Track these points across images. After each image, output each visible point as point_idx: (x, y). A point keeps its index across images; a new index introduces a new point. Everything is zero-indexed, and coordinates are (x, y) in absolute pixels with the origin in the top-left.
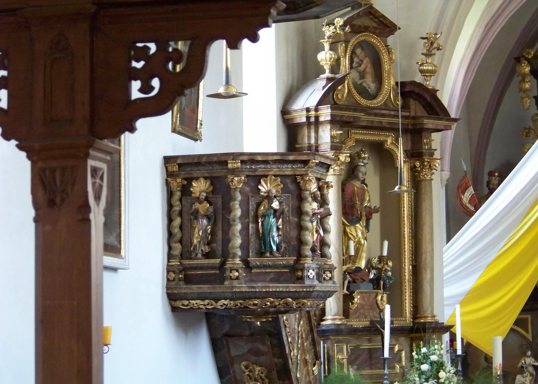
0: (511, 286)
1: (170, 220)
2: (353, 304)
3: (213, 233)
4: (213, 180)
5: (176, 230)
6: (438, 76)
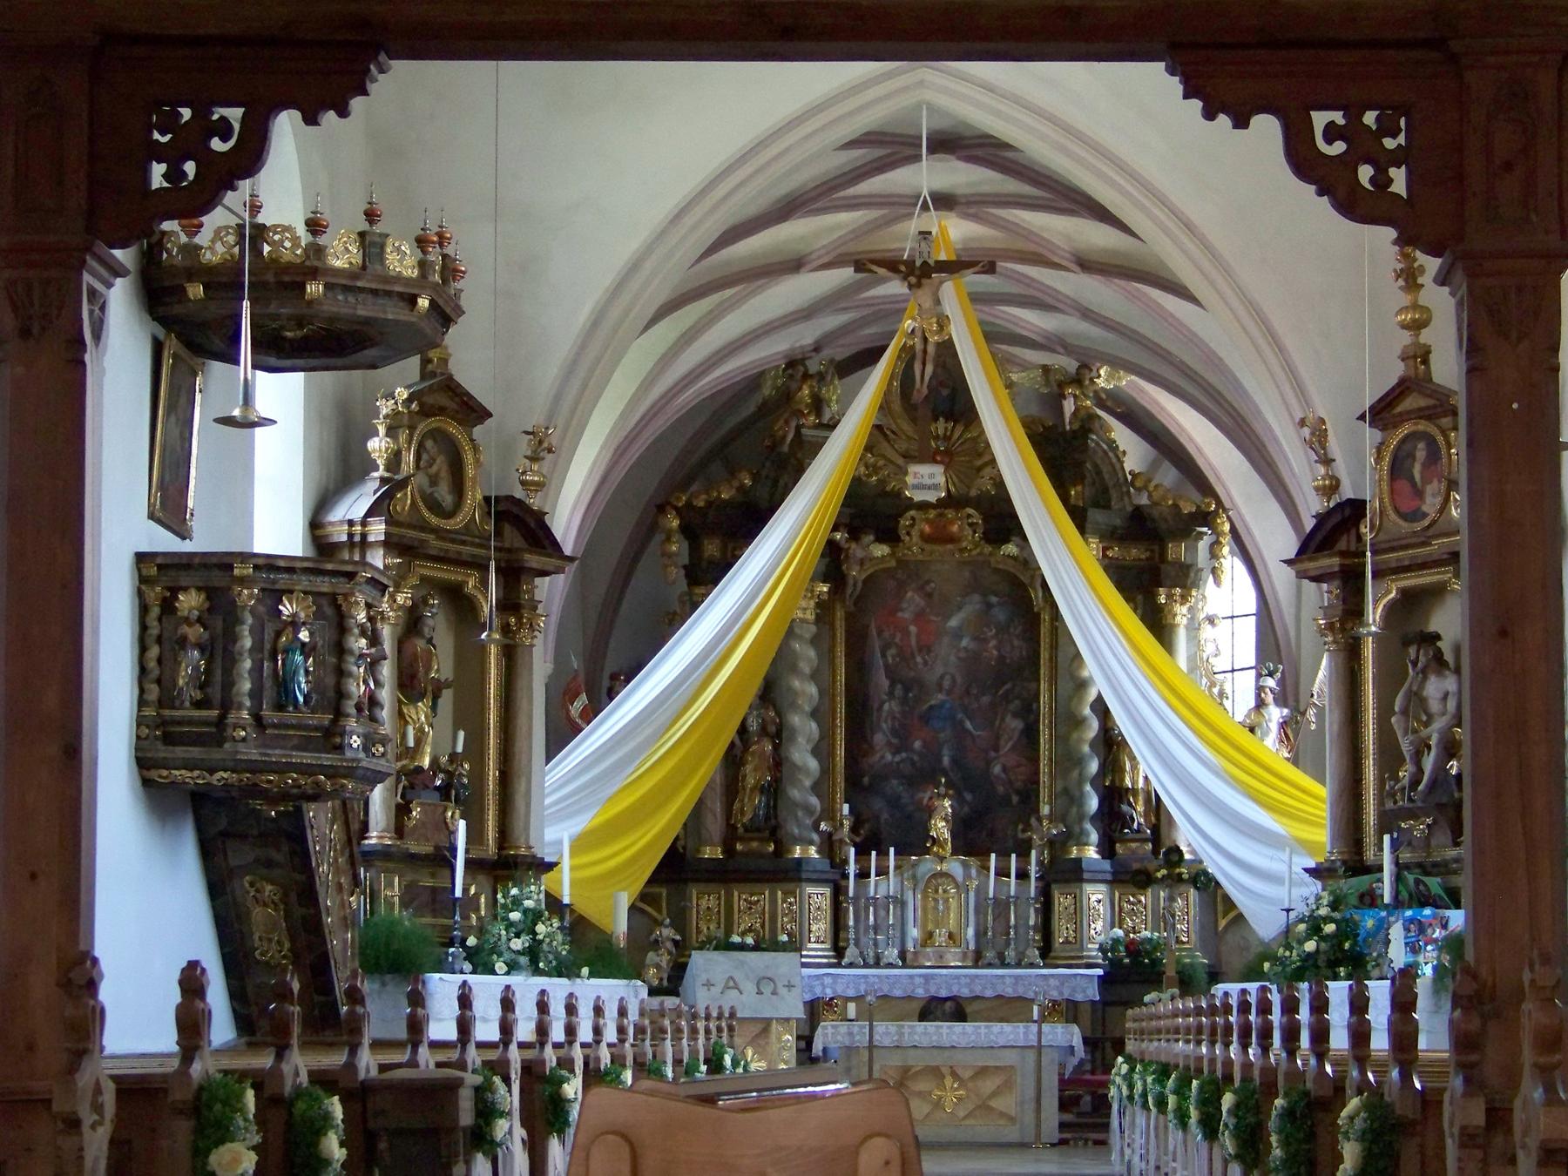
0: (638, 834)
1: (143, 648)
2: (409, 819)
3: (208, 671)
4: (211, 592)
5: (152, 664)
6: (546, 495)
